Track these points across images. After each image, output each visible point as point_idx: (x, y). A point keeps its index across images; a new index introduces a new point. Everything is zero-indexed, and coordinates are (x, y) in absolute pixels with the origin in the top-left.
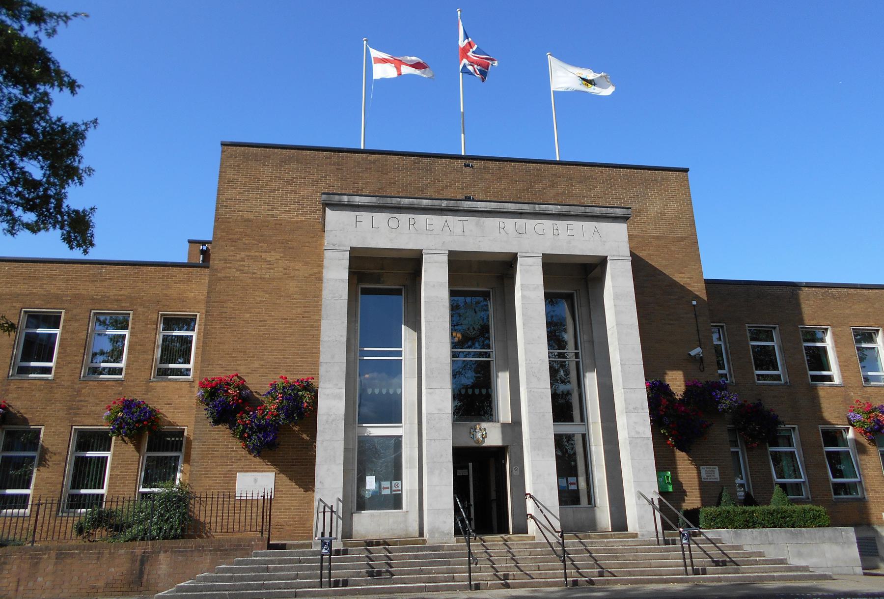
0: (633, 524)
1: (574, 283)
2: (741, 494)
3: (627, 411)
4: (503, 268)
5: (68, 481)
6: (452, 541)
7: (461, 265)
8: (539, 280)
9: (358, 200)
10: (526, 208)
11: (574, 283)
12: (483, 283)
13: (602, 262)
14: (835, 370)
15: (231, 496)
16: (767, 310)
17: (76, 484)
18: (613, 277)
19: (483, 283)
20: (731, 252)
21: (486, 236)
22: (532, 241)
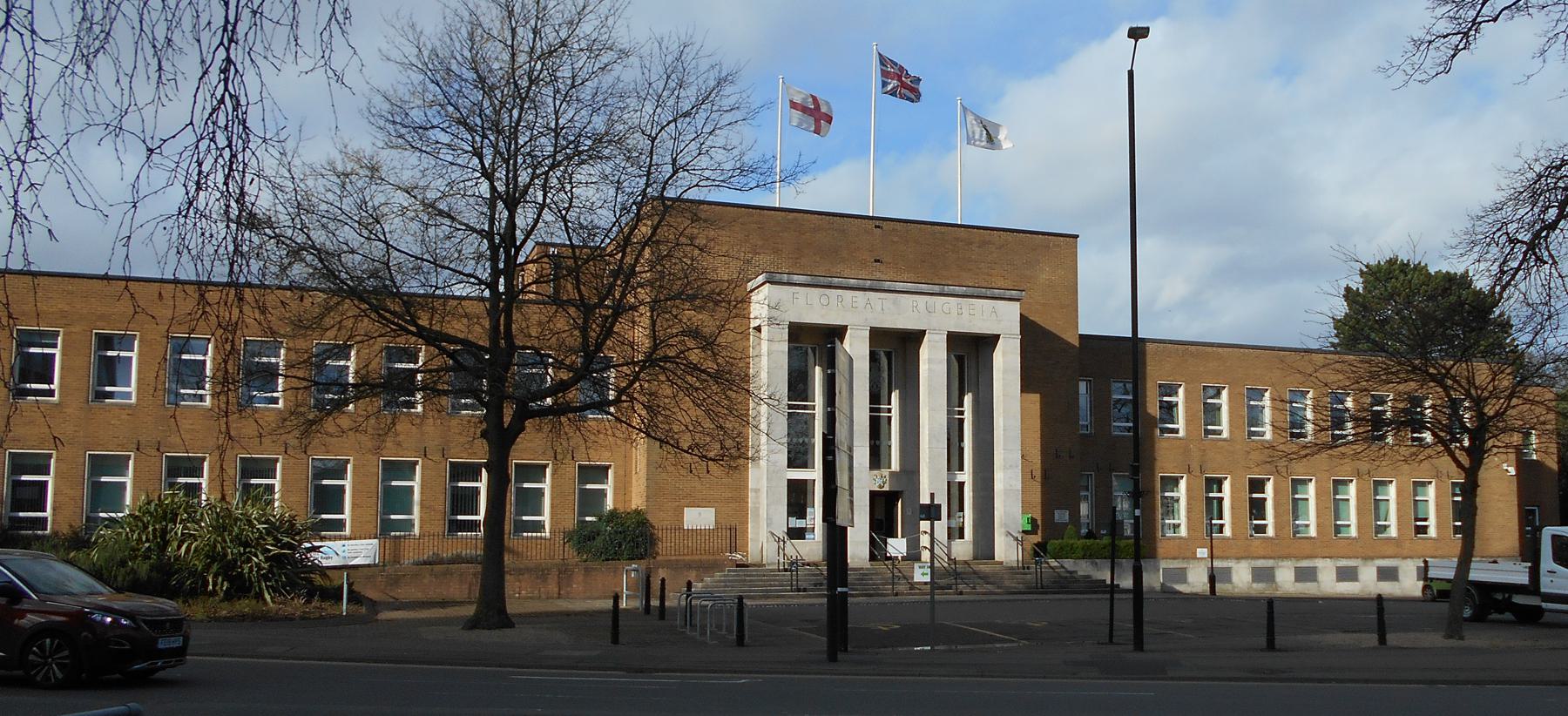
0: (999, 554)
1: (971, 352)
2: (1084, 531)
3: (1005, 468)
4: (912, 339)
5: (448, 509)
6: (868, 565)
7: (879, 336)
8: (943, 354)
9: (796, 278)
10: (937, 289)
11: (971, 352)
12: (893, 352)
13: (995, 339)
14: (1181, 425)
15: (681, 528)
16: (1123, 357)
17: (455, 512)
18: (1004, 354)
19: (893, 352)
20: (1100, 313)
21: (901, 312)
22: (938, 317)
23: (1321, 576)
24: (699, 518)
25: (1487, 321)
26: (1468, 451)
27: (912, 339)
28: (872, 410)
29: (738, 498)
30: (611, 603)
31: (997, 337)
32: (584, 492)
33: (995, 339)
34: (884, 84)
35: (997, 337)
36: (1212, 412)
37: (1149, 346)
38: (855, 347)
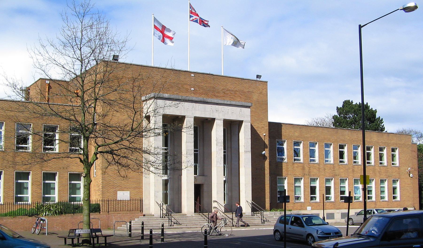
1: (232, 128)
7: (197, 120)
12: (203, 126)
13: (241, 122)
16: (276, 129)
23: (339, 216)
24: (123, 195)
25: (375, 120)
26: (84, 154)
27: (210, 122)
28: (195, 151)
29: (138, 187)
30: (140, 231)
31: (214, 120)
32: (17, 183)
33: (241, 122)
34: (191, 17)
35: (214, 120)
36: (312, 153)
37: (283, 127)
38: (189, 123)
